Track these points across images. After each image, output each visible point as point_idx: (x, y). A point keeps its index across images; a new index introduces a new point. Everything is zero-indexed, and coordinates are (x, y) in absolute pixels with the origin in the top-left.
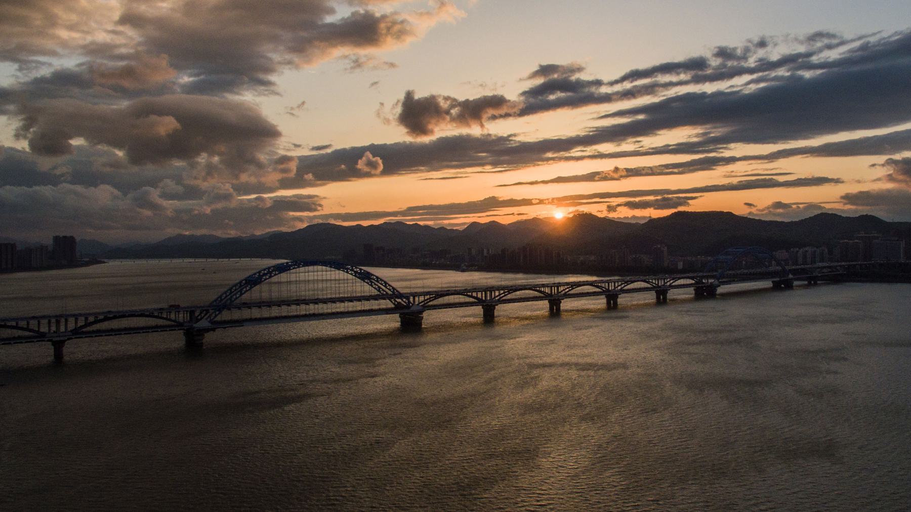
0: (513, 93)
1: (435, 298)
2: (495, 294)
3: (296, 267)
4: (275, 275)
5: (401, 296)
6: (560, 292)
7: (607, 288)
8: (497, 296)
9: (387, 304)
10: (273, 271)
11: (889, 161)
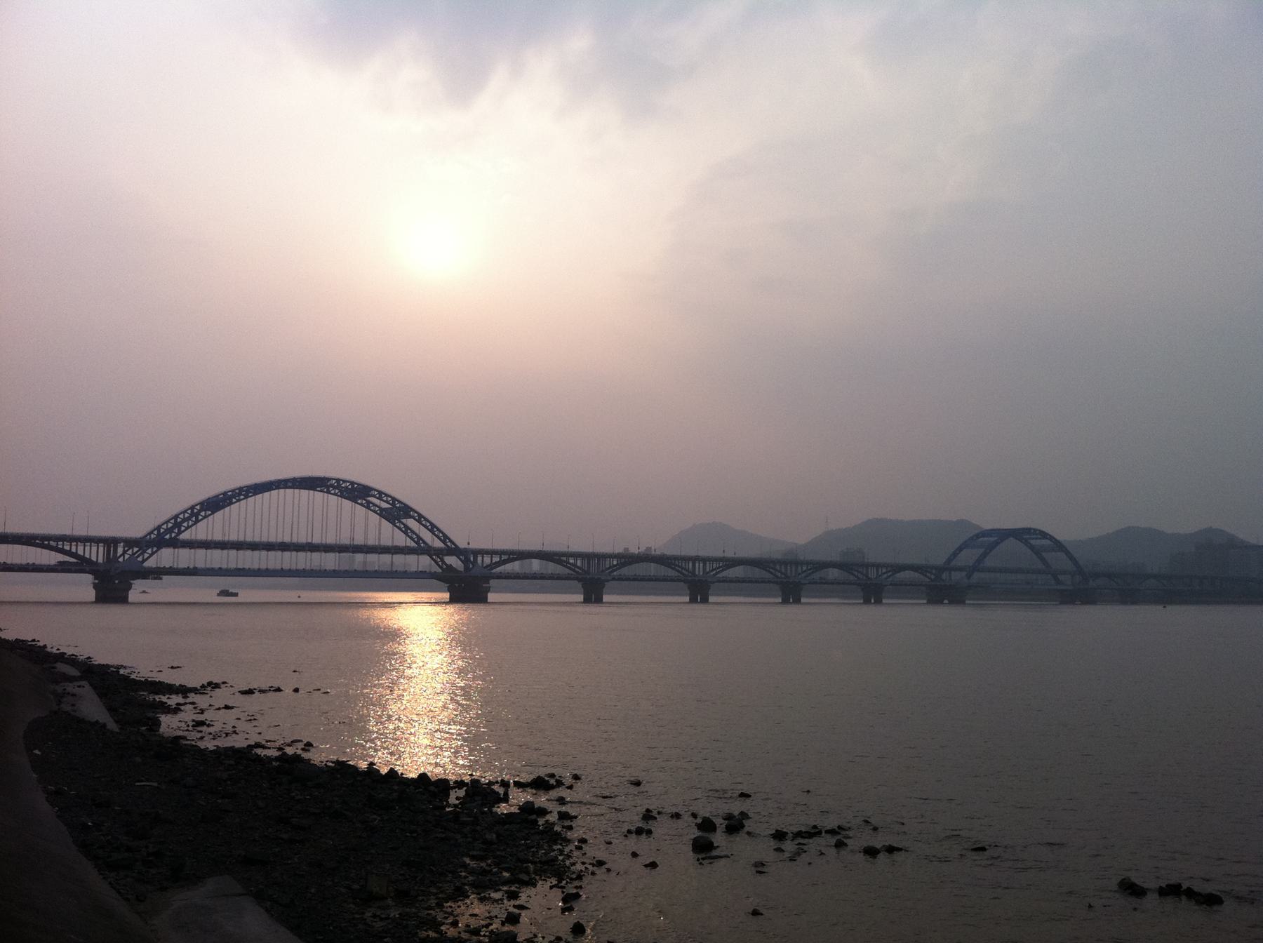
0: (257, 693)
1: (728, 567)
2: (796, 570)
3: (242, 497)
4: (205, 517)
5: (456, 551)
6: (708, 573)
7: (586, 569)
8: (884, 573)
9: (424, 562)
10: (200, 511)
11: (91, 708)
